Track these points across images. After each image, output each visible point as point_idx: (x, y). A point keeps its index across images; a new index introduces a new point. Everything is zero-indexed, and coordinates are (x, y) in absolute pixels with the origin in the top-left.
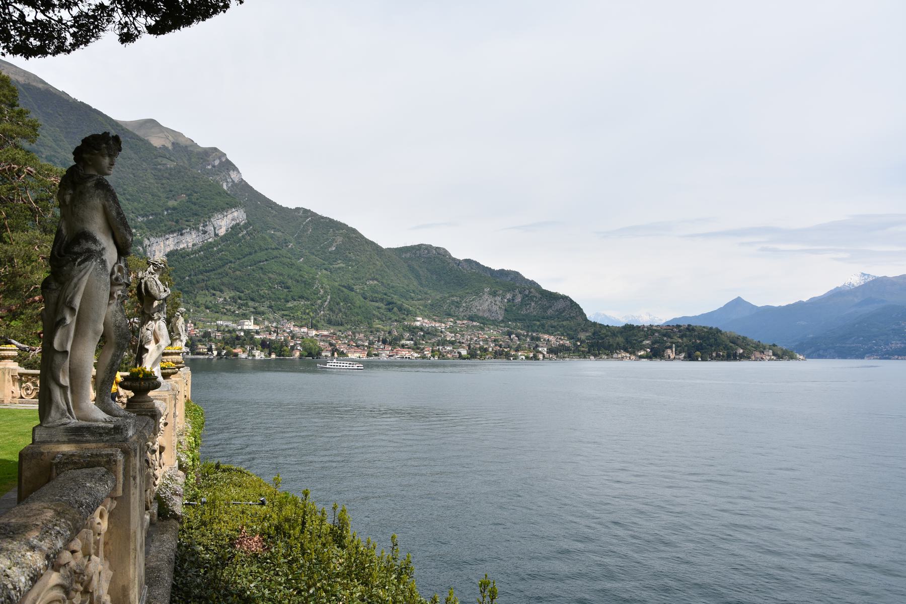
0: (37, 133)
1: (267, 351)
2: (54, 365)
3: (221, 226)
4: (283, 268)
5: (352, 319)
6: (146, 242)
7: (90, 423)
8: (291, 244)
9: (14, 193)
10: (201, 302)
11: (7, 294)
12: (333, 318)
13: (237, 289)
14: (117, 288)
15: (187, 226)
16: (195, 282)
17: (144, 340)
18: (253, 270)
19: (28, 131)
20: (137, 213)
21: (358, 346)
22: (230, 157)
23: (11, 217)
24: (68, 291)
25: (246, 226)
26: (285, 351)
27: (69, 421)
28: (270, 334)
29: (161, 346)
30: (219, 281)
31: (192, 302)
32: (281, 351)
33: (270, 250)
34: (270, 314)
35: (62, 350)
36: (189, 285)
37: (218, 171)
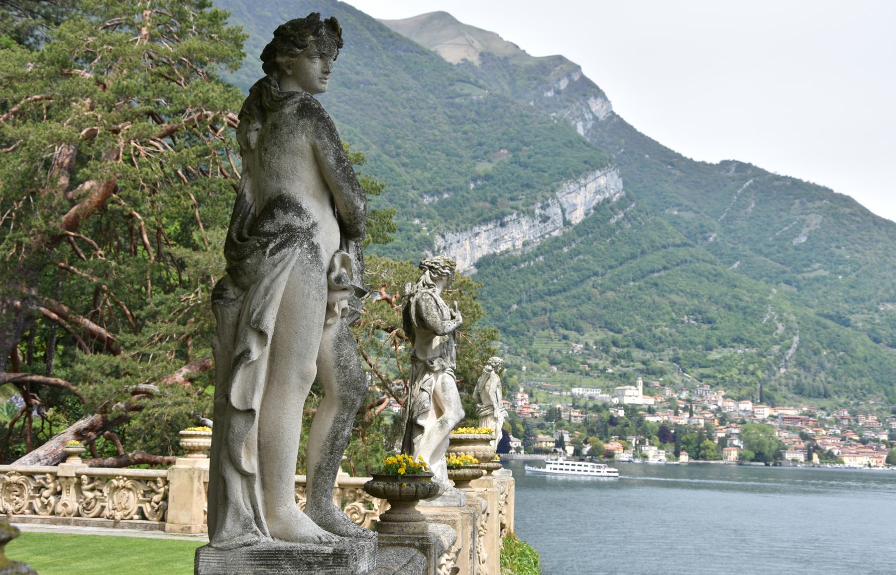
0: (242, 51)
1: (671, 447)
2: (231, 436)
3: (575, 205)
4: (700, 282)
5: (850, 383)
6: (439, 242)
7: (293, 544)
8: (714, 235)
9: (208, 161)
10: (541, 352)
11: (199, 340)
12: (807, 381)
13: (608, 326)
14: (338, 295)
15: (513, 208)
16: (531, 315)
17: (416, 410)
18: (640, 289)
19: (227, 48)
20: (422, 189)
21: (864, 442)
22: (588, 72)
23: (204, 203)
24: (254, 302)
25: (622, 204)
26: (707, 447)
27: (256, 538)
28: (676, 414)
29: (446, 422)
30: (575, 310)
31: (525, 351)
32: (700, 449)
33: (671, 249)
34: (676, 375)
35: (245, 408)
36: (519, 321)
37: (567, 100)
